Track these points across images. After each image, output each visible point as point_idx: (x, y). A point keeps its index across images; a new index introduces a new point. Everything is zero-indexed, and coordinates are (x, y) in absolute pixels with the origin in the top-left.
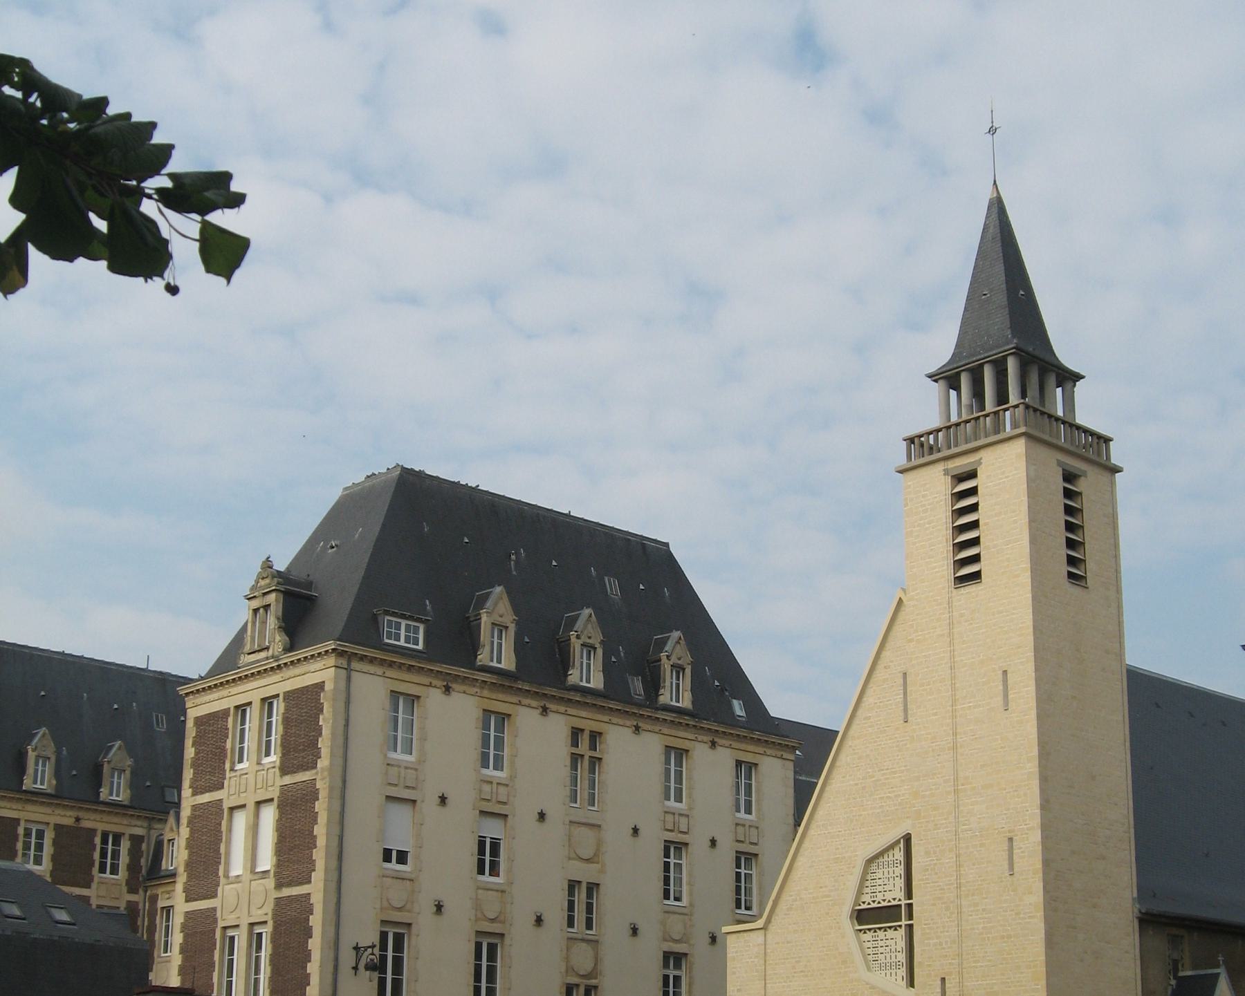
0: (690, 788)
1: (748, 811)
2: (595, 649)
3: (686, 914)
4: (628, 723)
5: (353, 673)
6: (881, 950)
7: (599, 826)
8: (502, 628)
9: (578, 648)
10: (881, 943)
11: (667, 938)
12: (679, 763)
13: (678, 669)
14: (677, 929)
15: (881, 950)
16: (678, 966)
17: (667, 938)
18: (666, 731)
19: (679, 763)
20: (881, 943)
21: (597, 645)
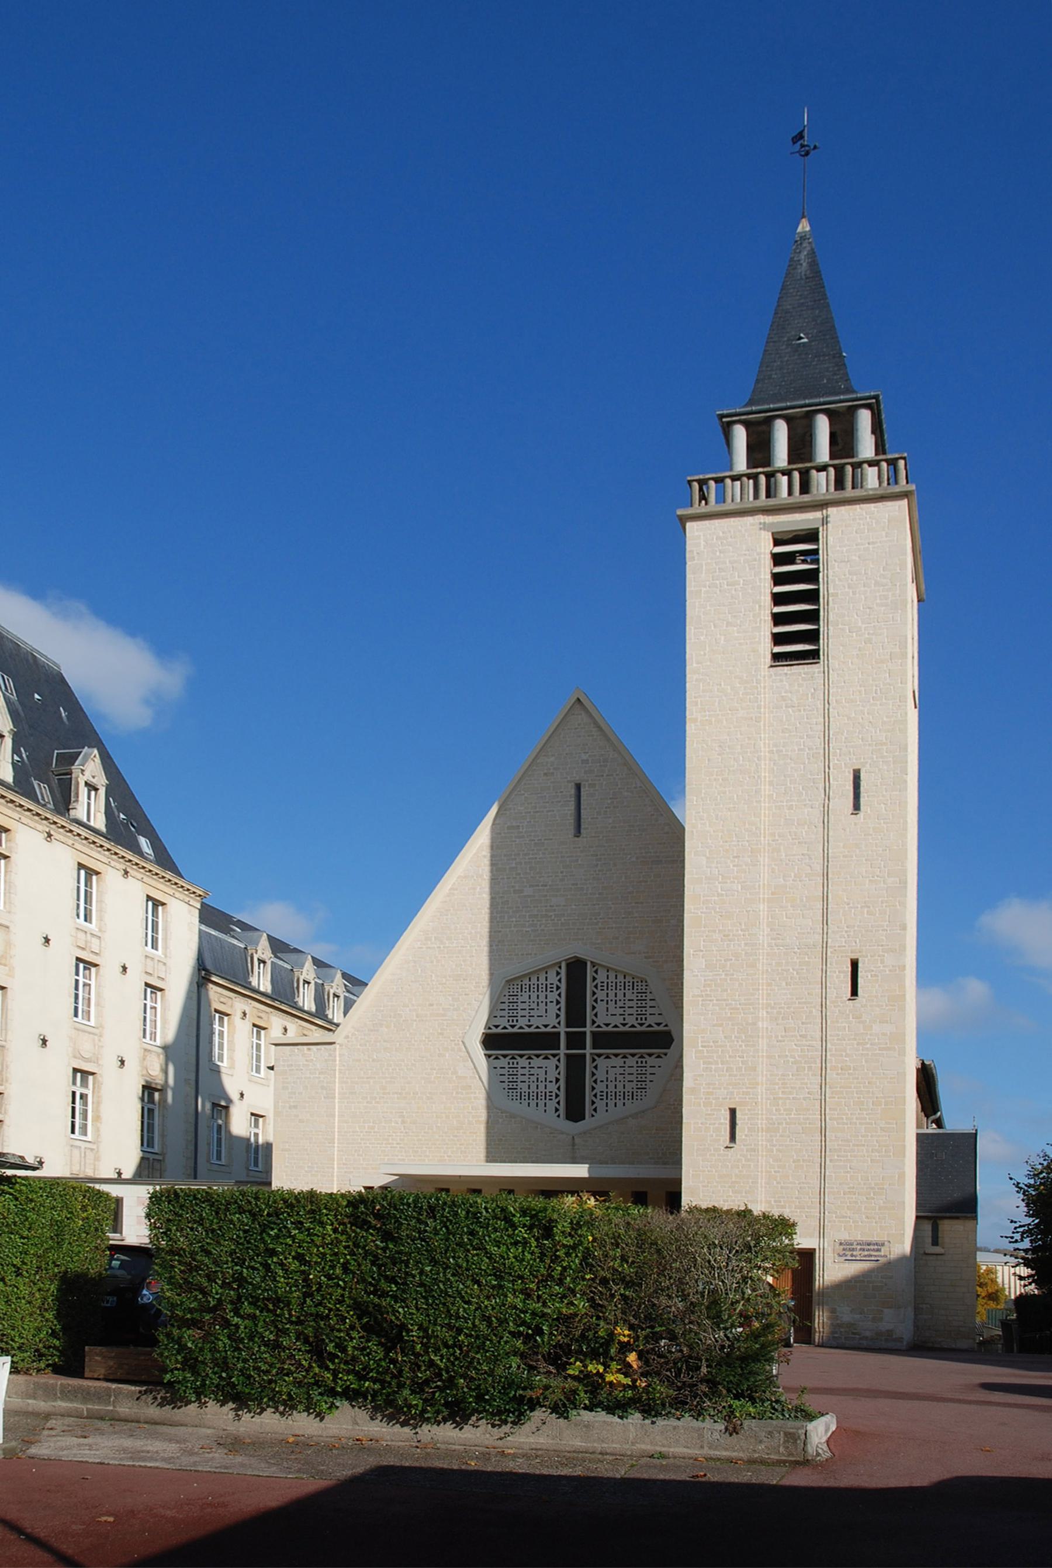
0: (100, 911)
1: (155, 946)
2: (96, 790)
3: (97, 1032)
4: (40, 827)
5: (940, 1222)
6: (620, 1088)
7: (8, 927)
8: (91, 787)
9: (82, 784)
10: (611, 1088)
11: (78, 1055)
12: (88, 882)
13: (91, 787)
14: (86, 1046)
15: (620, 1088)
16: (84, 1083)
17: (78, 1055)
18: (78, 846)
19: (88, 882)
20: (611, 1088)
21: (6, 734)
